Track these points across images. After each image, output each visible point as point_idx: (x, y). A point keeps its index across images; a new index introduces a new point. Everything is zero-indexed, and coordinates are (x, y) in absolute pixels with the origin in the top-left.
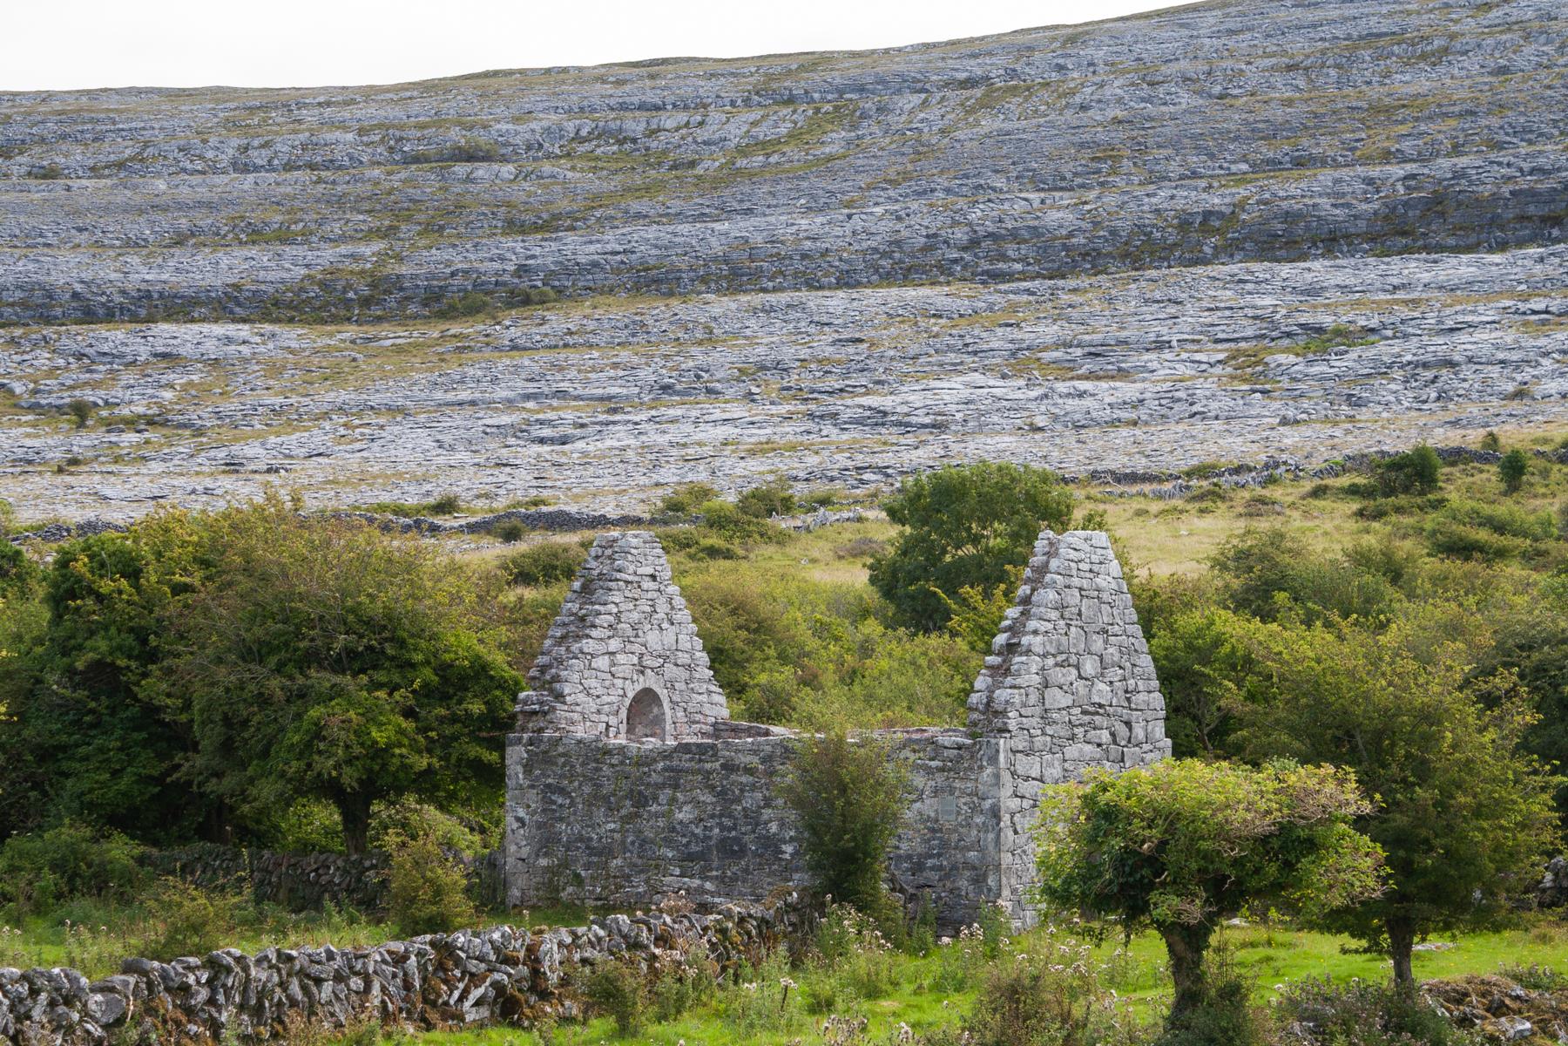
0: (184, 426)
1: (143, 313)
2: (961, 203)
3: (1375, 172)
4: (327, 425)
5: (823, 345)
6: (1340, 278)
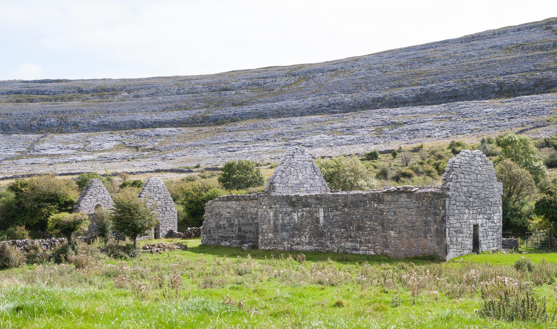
0: (158, 150)
1: (155, 126)
2: (327, 97)
3: (414, 88)
4: (187, 149)
5: (292, 129)
6: (402, 112)
